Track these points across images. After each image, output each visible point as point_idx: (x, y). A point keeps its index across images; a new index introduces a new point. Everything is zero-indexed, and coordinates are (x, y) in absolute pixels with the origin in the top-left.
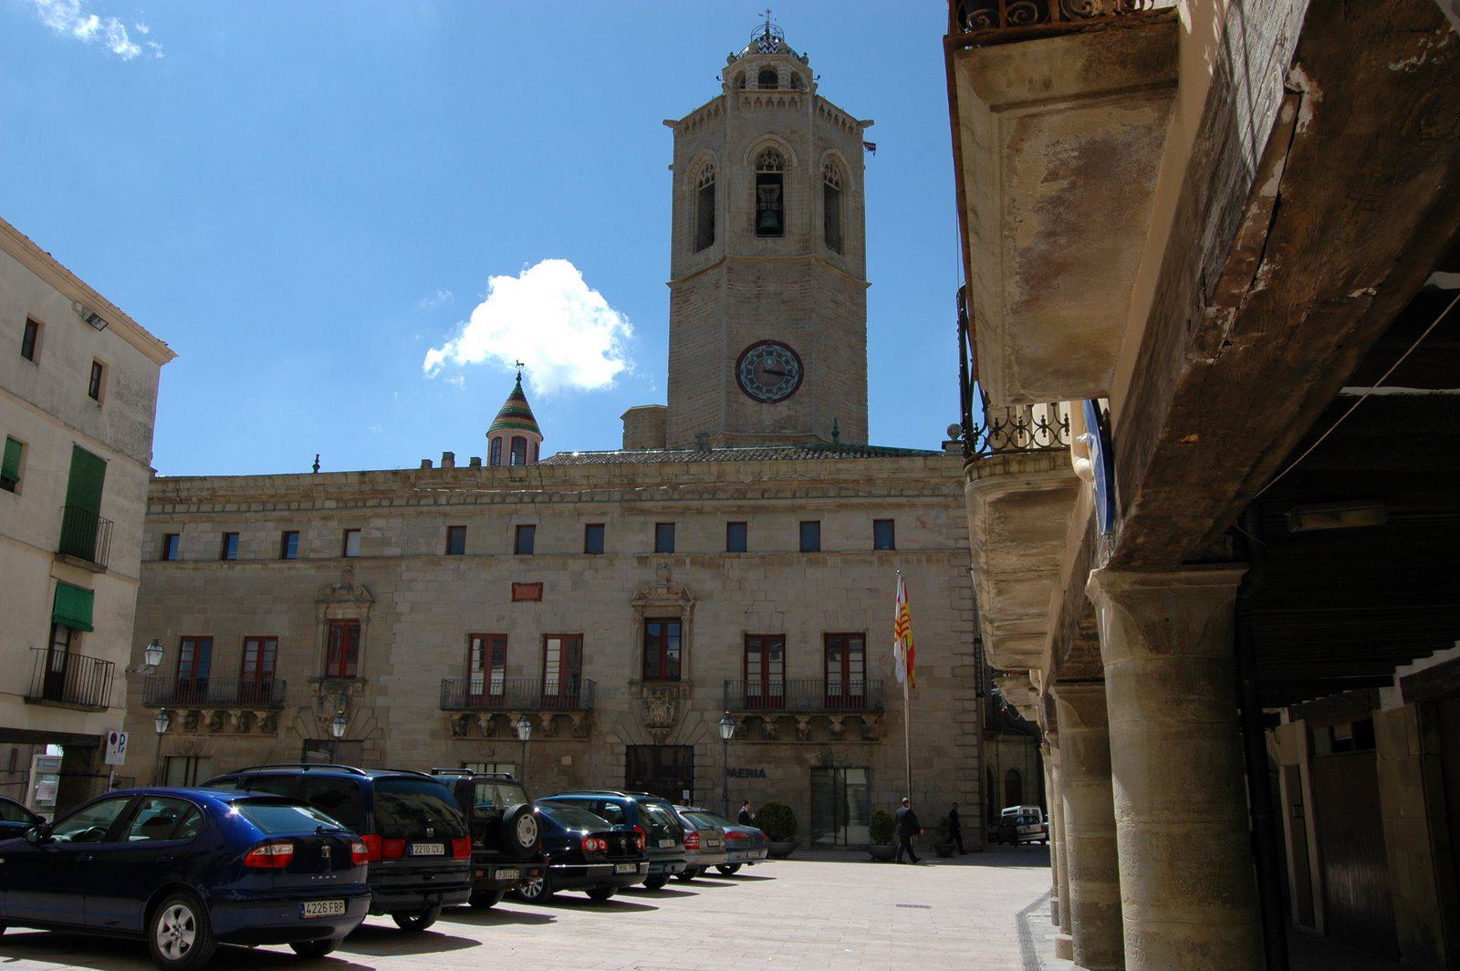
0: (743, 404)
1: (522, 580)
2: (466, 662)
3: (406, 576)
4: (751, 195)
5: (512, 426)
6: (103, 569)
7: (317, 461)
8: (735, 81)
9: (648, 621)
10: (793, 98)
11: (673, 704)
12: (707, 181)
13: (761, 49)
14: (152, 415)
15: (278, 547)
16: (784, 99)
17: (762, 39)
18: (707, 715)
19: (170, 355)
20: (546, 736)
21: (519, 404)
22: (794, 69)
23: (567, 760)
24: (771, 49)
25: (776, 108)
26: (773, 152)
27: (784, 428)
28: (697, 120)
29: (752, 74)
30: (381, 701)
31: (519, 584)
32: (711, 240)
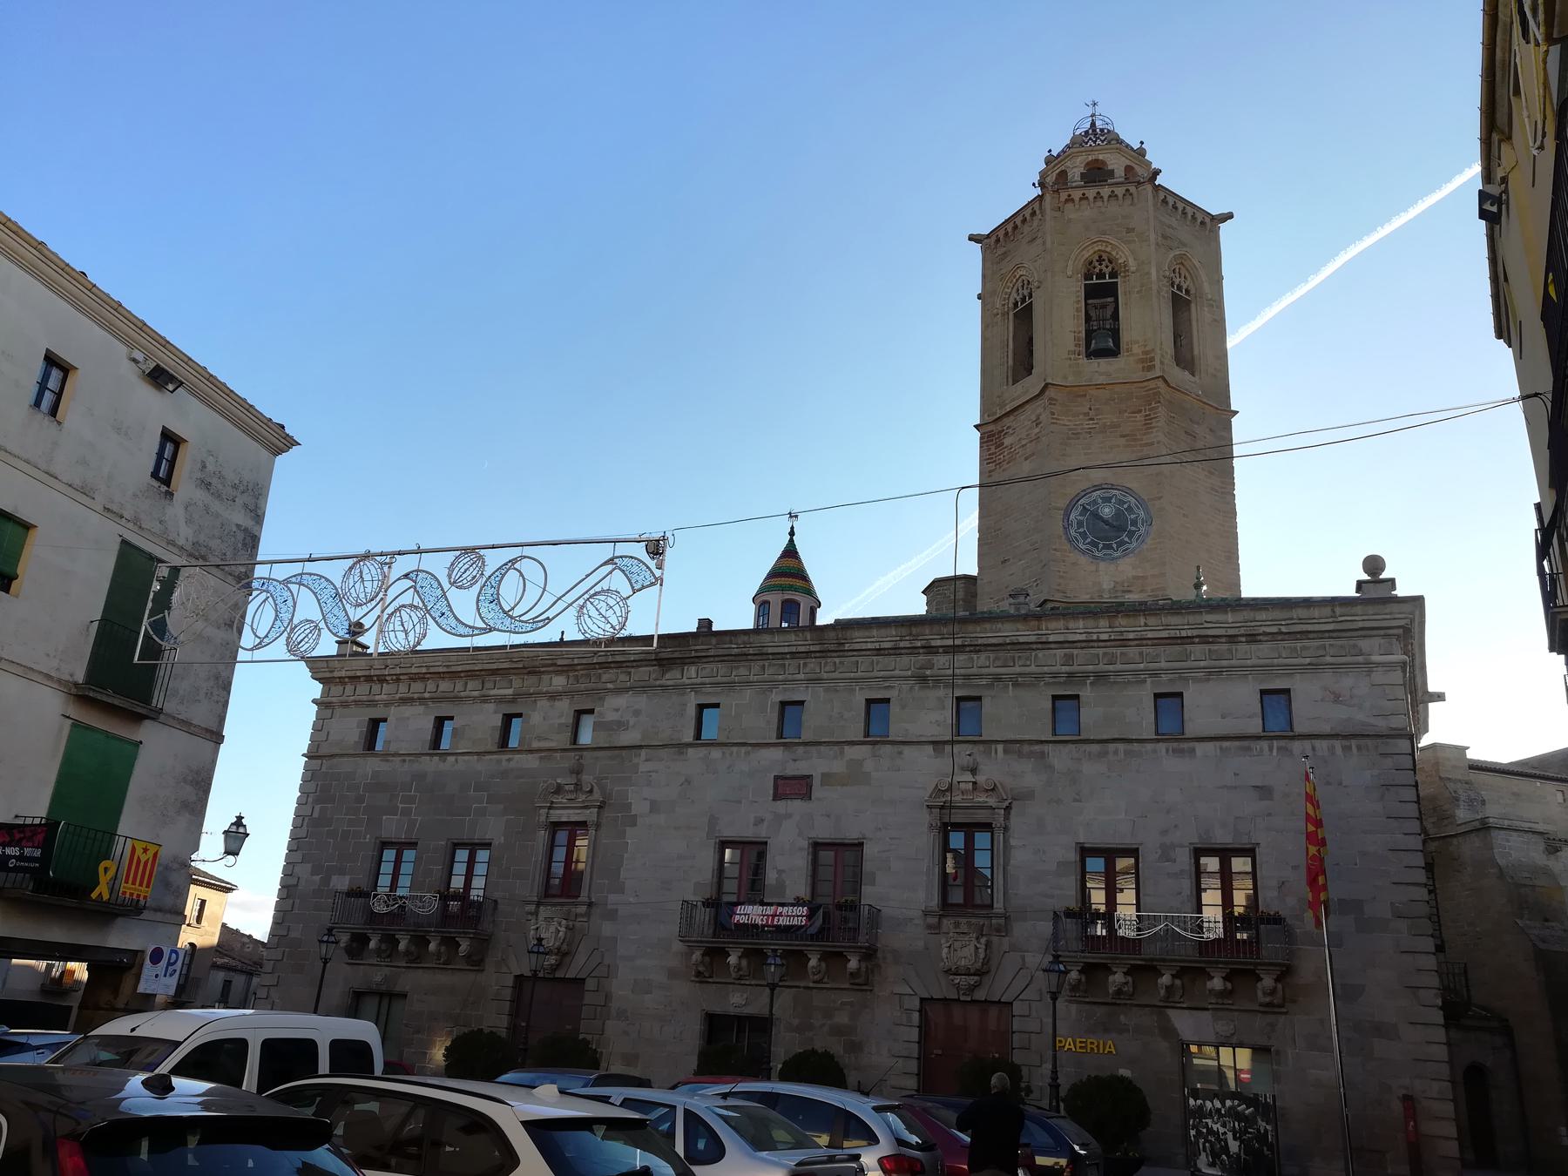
0: (1074, 564)
3: (644, 767)
4: (1078, 310)
5: (782, 588)
6: (155, 715)
8: (1055, 177)
10: (1127, 190)
11: (983, 940)
12: (1023, 300)
13: (1087, 143)
14: (259, 518)
15: (497, 735)
17: (1086, 132)
19: (290, 443)
21: (790, 562)
22: (1128, 163)
24: (1098, 142)
26: (1105, 256)
28: (1010, 230)
29: (1076, 171)
30: (607, 929)
32: (1029, 369)
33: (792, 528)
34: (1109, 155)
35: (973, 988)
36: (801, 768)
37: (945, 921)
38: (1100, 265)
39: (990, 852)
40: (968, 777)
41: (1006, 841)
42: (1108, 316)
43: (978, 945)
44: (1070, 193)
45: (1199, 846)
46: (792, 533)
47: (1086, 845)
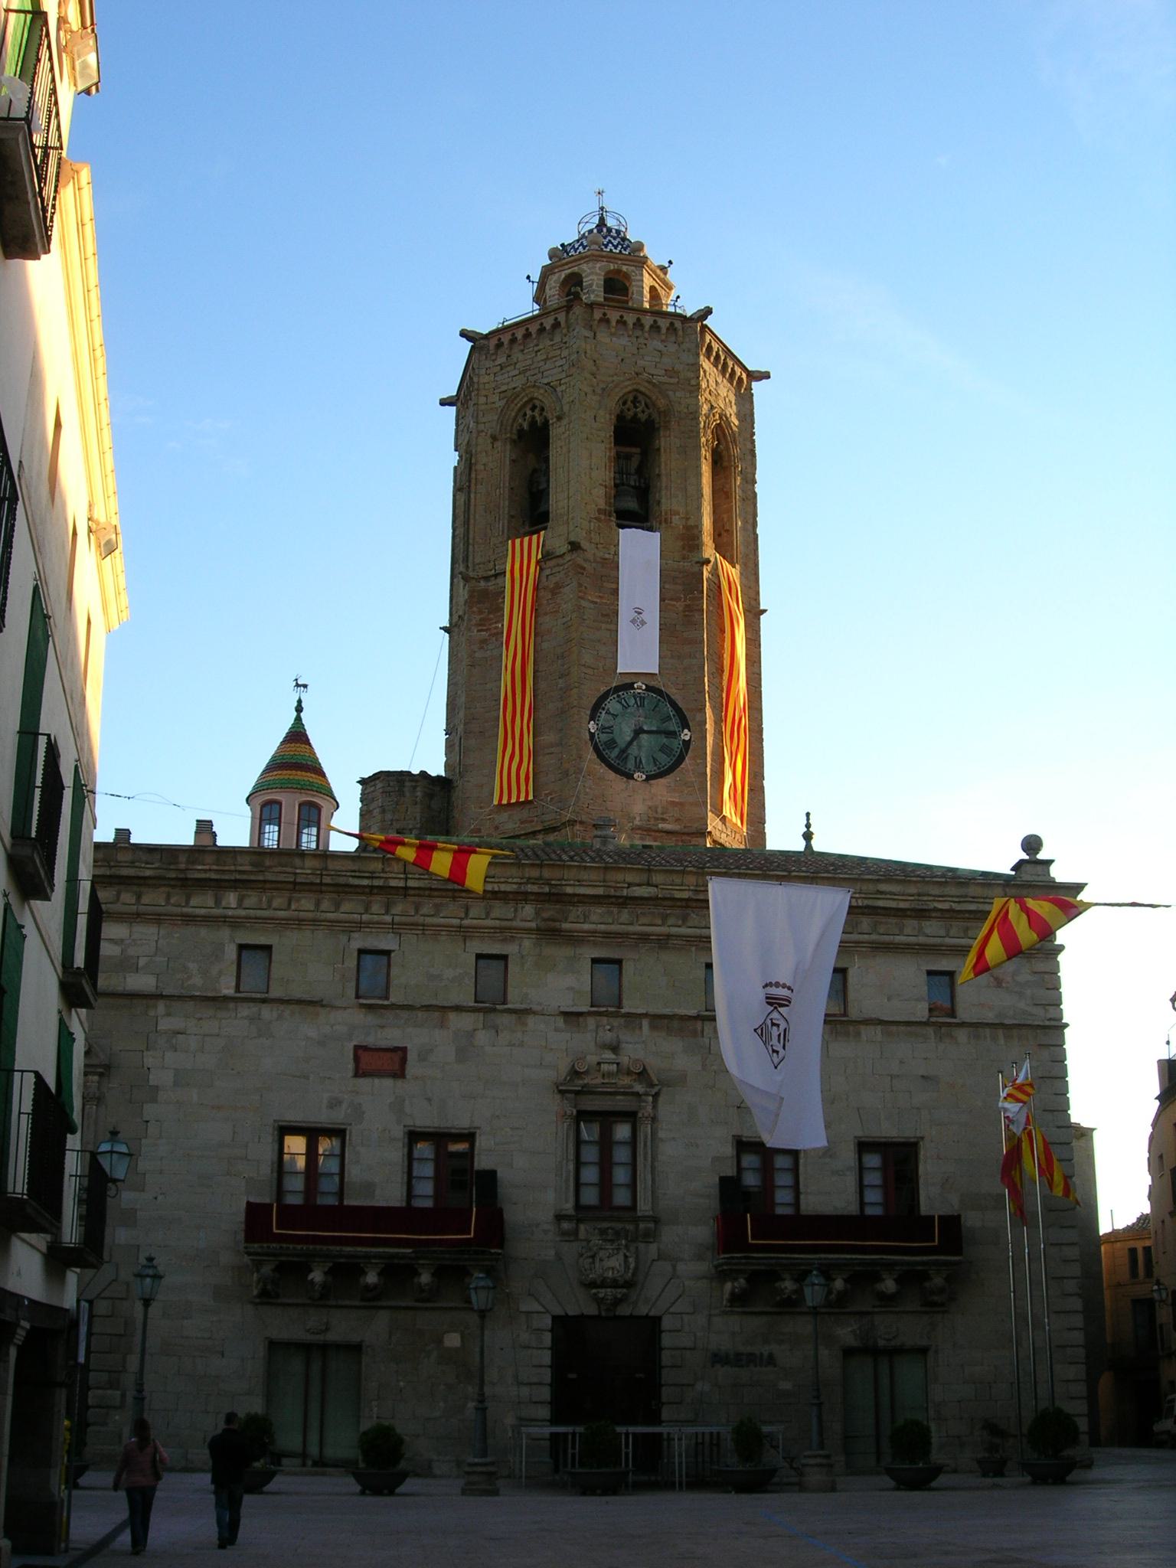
1: (370, 1041)
2: (275, 1175)
3: (165, 1024)
7: (808, 826)
9: (582, 1116)
13: (606, 247)
16: (643, 321)
18: (681, 1267)
20: (417, 1301)
23: (453, 1340)
25: (646, 335)
27: (664, 820)
31: (365, 1048)
33: (300, 701)
34: (633, 268)
35: (617, 1302)
36: (390, 1036)
37: (582, 1227)
38: (636, 407)
39: (22, 1111)
40: (609, 1055)
41: (654, 1133)
42: (633, 471)
43: (628, 1254)
44: (606, 311)
45: (863, 1139)
46: (299, 709)
47: (744, 1139)
